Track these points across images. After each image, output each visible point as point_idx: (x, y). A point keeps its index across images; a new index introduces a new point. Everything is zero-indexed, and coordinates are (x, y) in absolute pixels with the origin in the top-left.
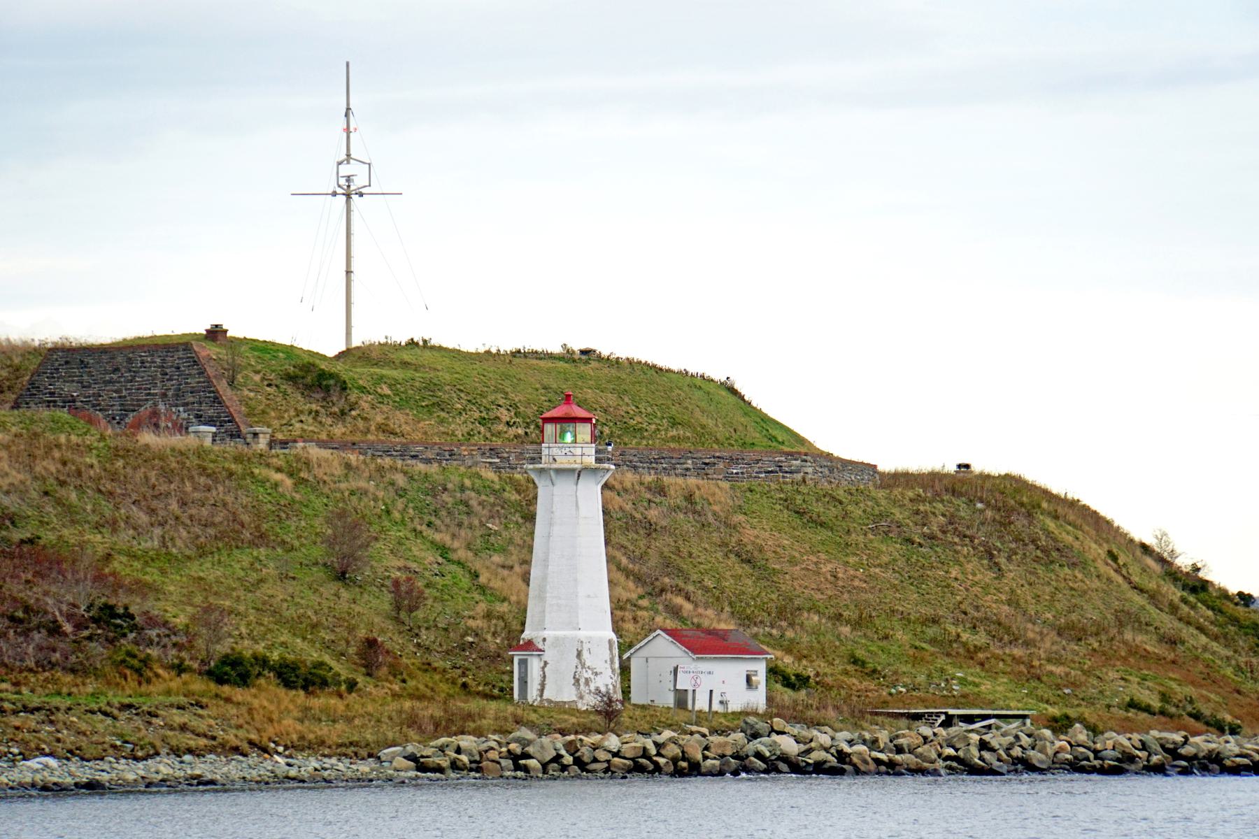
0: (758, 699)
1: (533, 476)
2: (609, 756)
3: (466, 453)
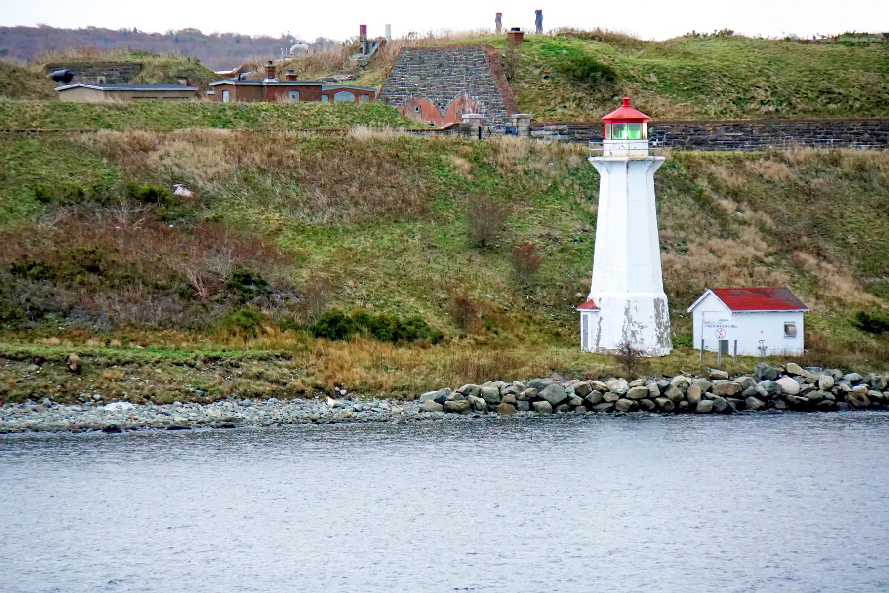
0: (796, 346)
1: (596, 166)
3: (711, 129)
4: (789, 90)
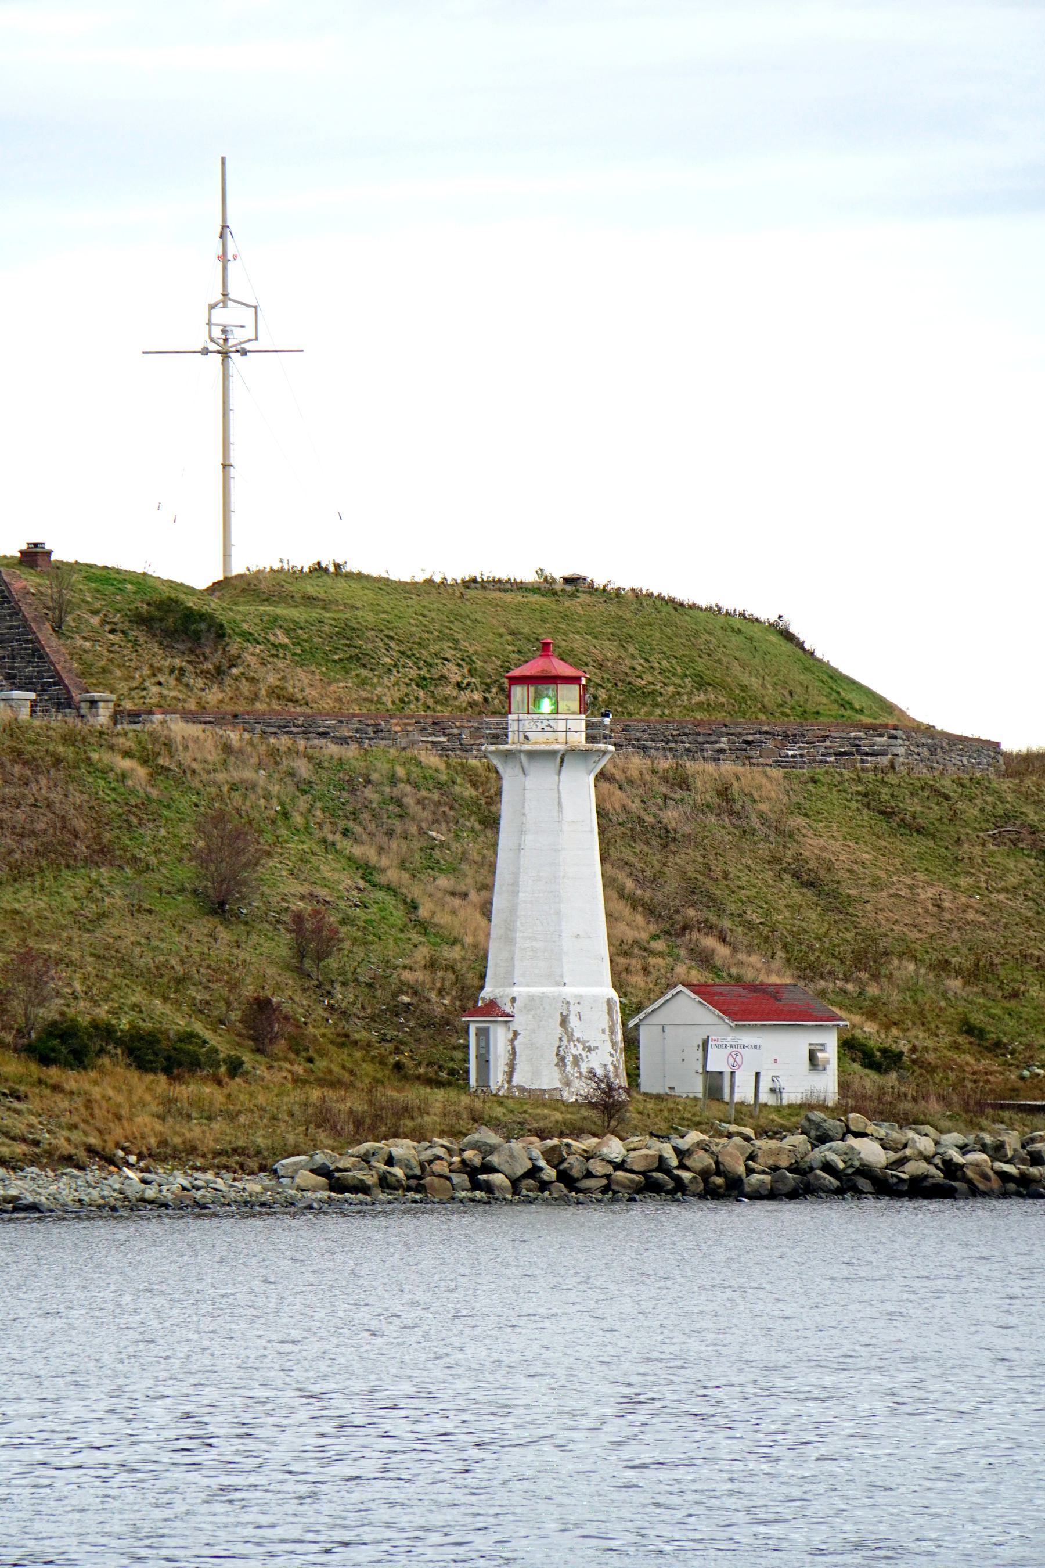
2: (610, 1169)
3: (398, 728)
4: (494, 666)
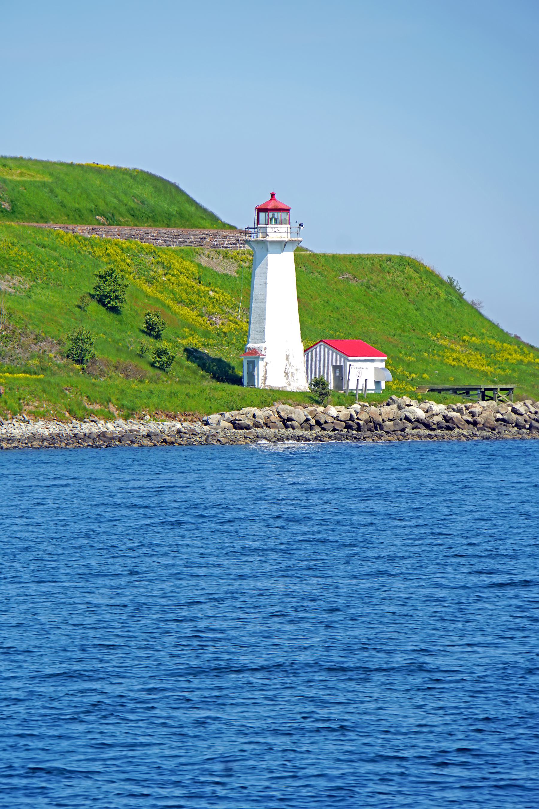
3: (80, 231)
